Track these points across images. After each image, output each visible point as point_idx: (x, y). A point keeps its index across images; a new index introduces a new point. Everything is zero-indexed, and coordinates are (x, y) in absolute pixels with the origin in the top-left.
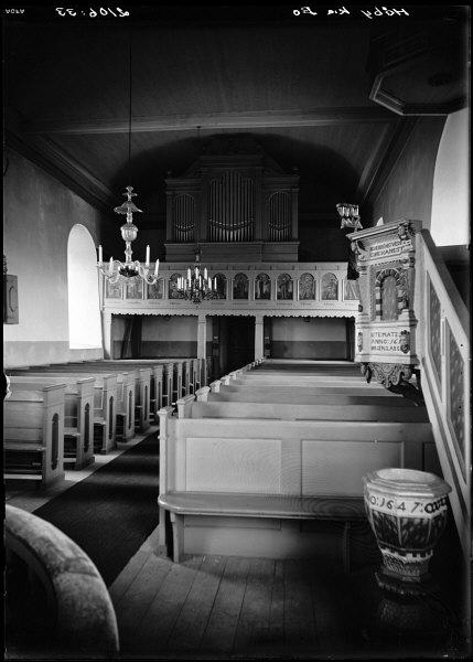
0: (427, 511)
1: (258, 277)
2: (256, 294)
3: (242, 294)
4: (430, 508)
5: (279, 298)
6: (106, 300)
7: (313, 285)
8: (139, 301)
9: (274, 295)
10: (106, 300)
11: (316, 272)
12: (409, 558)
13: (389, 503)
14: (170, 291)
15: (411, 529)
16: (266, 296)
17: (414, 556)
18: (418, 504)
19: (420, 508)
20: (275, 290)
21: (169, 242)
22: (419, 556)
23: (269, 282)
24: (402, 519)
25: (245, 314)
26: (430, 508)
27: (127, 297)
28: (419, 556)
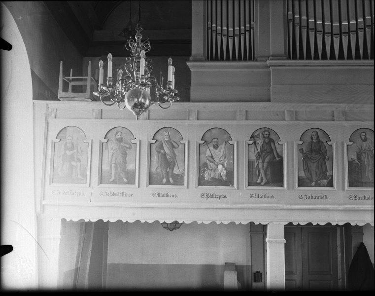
14: (202, 168)
27: (151, 182)
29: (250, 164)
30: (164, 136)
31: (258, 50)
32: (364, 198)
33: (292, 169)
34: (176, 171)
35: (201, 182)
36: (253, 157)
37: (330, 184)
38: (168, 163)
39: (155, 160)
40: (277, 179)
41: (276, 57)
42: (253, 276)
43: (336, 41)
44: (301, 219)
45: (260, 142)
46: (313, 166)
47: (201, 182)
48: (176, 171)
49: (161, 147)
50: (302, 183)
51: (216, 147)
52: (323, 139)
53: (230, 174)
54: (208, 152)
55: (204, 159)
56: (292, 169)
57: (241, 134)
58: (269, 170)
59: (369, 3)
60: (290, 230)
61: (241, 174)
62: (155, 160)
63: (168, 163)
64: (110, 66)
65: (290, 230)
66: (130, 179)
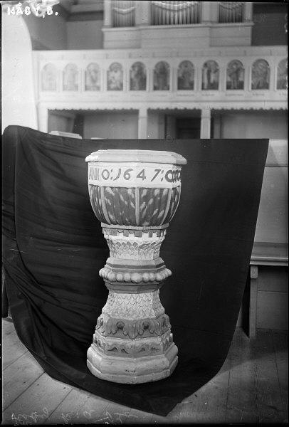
0: (169, 181)
1: (206, 65)
2: (203, 84)
3: (187, 85)
4: (170, 176)
5: (229, 87)
6: (41, 93)
7: (266, 74)
8: (75, 93)
9: (223, 85)
10: (41, 93)
11: (271, 58)
12: (145, 238)
13: (126, 173)
14: (109, 83)
15: (151, 201)
16: (214, 86)
17: (151, 236)
18: (159, 171)
19: (161, 175)
20: (223, 79)
21: (107, 27)
22: (155, 235)
23: (217, 71)
24: (141, 189)
25: (190, 106)
26: (170, 176)
27: (64, 89)
28: (155, 235)
29: (131, 80)
30: (92, 67)
31: (137, 21)
32: (253, 260)
33: (150, 83)
34: (98, 84)
35: (109, 89)
36: (133, 76)
37: (168, 89)
38: (94, 81)
39: (88, 78)
40: (143, 86)
41: (144, 24)
42: (225, 25)
43: (176, 14)
44: (155, 106)
45: (136, 69)
46: (161, 80)
47: (109, 89)
48: (98, 84)
49: (90, 73)
50: (155, 88)
51: (116, 72)
52: (166, 67)
53: (122, 85)
54: (112, 74)
55: (110, 78)
56: (150, 83)
57: (127, 65)
58: (139, 81)
59: (135, 264)
60: (150, 112)
61: (126, 85)
62: (88, 78)
63: (94, 81)
64: (198, 84)
65: (150, 112)
66: (76, 88)
